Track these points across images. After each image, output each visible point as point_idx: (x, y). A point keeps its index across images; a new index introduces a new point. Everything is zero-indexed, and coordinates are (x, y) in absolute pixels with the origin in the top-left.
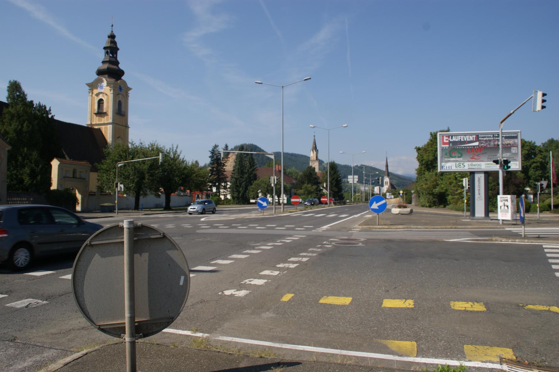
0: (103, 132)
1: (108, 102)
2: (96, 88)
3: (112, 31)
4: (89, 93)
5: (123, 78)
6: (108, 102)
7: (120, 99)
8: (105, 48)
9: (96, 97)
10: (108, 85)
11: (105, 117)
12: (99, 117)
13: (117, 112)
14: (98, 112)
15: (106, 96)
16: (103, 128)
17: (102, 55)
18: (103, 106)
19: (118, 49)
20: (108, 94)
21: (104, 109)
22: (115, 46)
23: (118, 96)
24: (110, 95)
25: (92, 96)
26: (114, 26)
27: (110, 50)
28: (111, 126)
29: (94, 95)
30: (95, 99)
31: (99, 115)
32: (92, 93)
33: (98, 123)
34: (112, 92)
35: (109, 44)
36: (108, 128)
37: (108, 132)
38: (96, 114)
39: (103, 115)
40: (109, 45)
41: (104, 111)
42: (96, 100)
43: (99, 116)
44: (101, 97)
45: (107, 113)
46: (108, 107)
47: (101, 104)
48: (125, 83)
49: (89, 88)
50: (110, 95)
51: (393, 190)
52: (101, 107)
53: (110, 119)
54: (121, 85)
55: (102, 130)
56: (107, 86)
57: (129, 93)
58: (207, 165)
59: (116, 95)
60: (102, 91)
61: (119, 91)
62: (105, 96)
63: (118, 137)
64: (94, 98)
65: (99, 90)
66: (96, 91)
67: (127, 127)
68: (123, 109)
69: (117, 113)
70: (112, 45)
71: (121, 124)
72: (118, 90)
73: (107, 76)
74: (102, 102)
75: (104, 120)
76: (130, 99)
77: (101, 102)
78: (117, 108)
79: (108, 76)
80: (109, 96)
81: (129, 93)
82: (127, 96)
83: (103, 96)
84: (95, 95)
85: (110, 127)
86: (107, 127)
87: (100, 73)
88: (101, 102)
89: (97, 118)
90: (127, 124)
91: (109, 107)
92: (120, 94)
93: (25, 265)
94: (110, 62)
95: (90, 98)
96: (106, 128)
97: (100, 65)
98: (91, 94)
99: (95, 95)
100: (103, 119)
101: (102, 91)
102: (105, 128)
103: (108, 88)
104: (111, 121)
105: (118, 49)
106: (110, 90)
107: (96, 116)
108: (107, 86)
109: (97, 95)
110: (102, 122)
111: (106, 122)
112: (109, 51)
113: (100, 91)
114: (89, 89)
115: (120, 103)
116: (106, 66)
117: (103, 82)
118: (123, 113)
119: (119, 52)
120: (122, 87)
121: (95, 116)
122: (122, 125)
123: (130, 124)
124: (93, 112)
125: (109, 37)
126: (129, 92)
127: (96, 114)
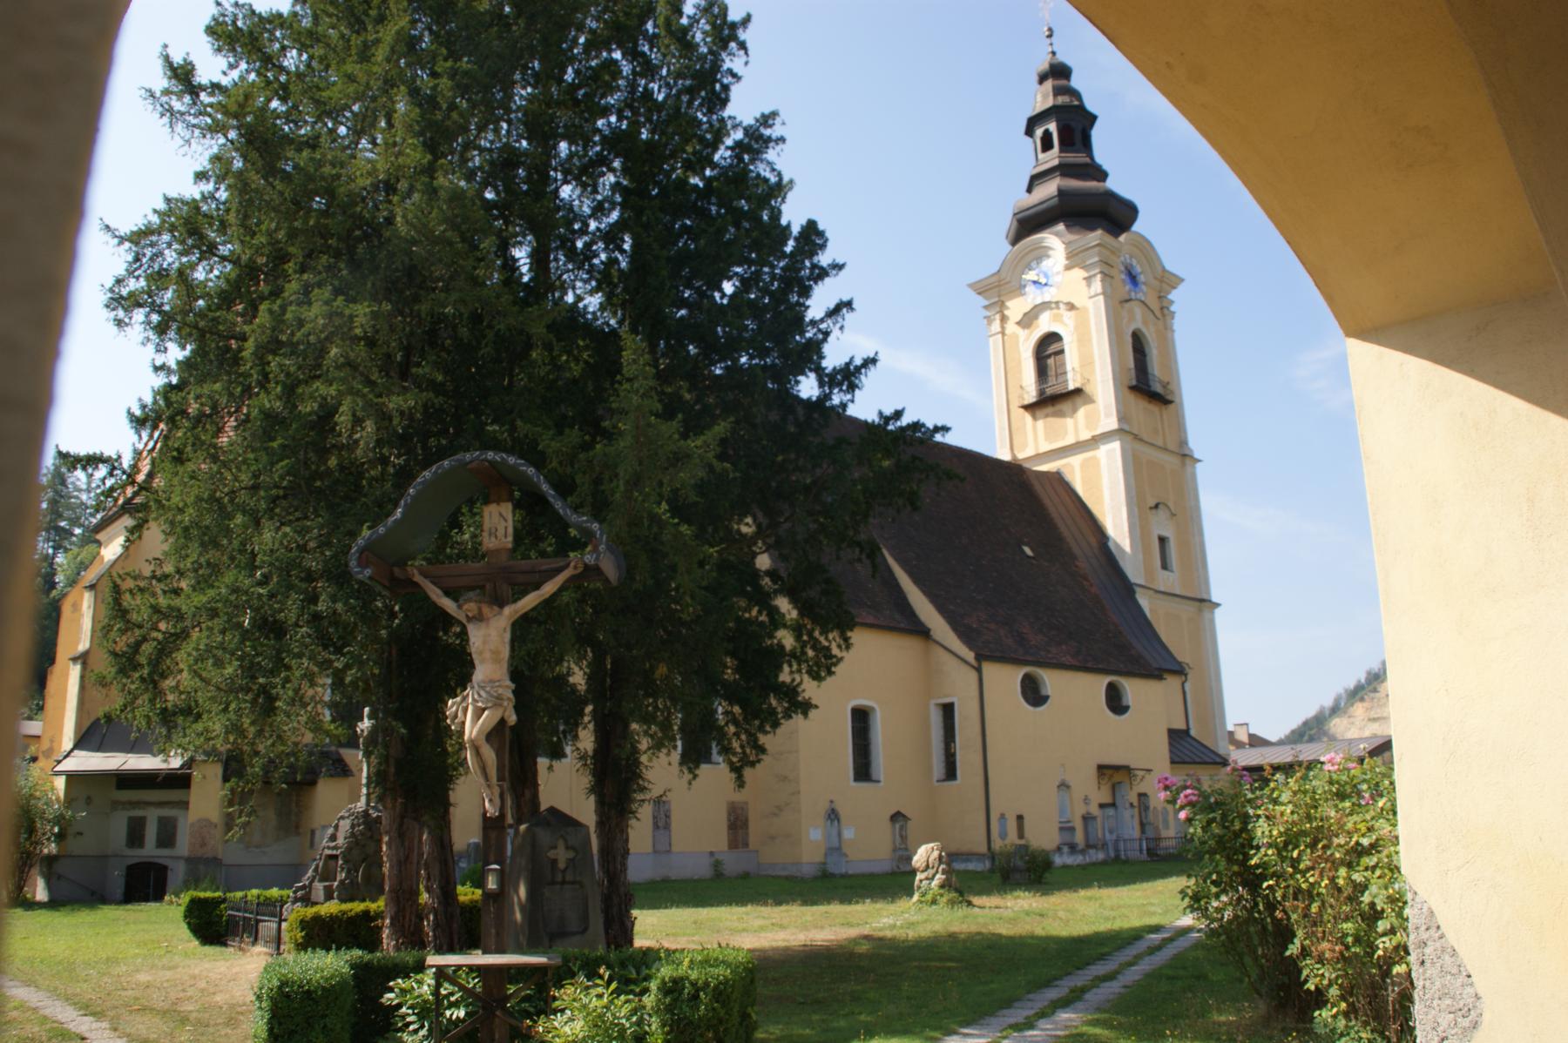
0: (1079, 488)
1: (1083, 339)
2: (1019, 289)
3: (1054, 53)
4: (989, 320)
5: (1136, 227)
6: (1083, 339)
7: (1138, 324)
8: (1032, 124)
9: (1022, 333)
10: (1075, 258)
11: (1082, 412)
12: (1051, 420)
13: (1134, 383)
14: (1041, 392)
15: (1073, 313)
16: (1075, 471)
17: (1026, 156)
18: (1063, 364)
19: (1092, 119)
20: (1077, 304)
21: (1070, 376)
22: (1076, 103)
23: (1127, 305)
24: (1090, 304)
25: (1003, 333)
26: (1055, 34)
27: (1058, 122)
28: (1115, 446)
29: (1011, 327)
30: (1017, 342)
31: (1050, 409)
32: (1004, 319)
33: (1045, 447)
34: (1097, 285)
35: (1051, 98)
36: (1103, 461)
37: (1105, 481)
38: (1028, 408)
39: (1065, 406)
40: (1050, 103)
41: (1071, 387)
42: (1027, 344)
43: (1047, 416)
44: (1045, 325)
45: (1088, 389)
46: (1086, 362)
47: (1051, 361)
48: (1145, 248)
49: (986, 303)
50: (1090, 304)
51: (268, 927)
52: (1051, 372)
53: (1107, 416)
54: (1134, 262)
55: (1068, 477)
56: (1068, 268)
57: (1172, 302)
58: (1327, 713)
59: (1116, 306)
60: (1047, 299)
61: (1128, 287)
62: (1068, 316)
63: (1156, 506)
64: (1016, 336)
65: (1032, 297)
66: (1016, 308)
67: (1185, 457)
68: (1156, 368)
69: (1133, 388)
70: (1061, 100)
71: (1160, 443)
72: (1123, 281)
73: (1061, 227)
74: (1053, 348)
75: (1075, 425)
76: (1179, 324)
77: (1047, 350)
78: (1131, 364)
79: (1067, 226)
80: (1085, 310)
81: (1172, 302)
82: (1163, 313)
83: (1058, 319)
84: (1018, 323)
85: (1111, 456)
86: (1095, 460)
87: (1029, 224)
88: (1047, 350)
89: (1040, 423)
90: (1183, 443)
91: (1092, 363)
92: (1130, 300)
93: (243, 66)
94: (1063, 170)
95: (995, 343)
96: (1091, 467)
97: (1017, 197)
98: (996, 326)
99: (1018, 323)
100: (1069, 421)
101: (1048, 295)
102: (1084, 465)
103: (1078, 274)
104: (1111, 423)
105: (1092, 119)
106: (1088, 279)
107: (1035, 418)
108: (1068, 268)
109: (1027, 320)
110: (1070, 440)
111: (1085, 435)
112: (1052, 127)
113: (1039, 301)
114: (986, 307)
115: (1139, 346)
116: (1049, 189)
117: (1048, 256)
118: (1158, 388)
119: (1097, 134)
120: (1139, 269)
121: (1028, 417)
122: (1166, 450)
123: (1196, 444)
124: (1015, 404)
125: (1042, 78)
126: (1170, 297)
127: (1028, 408)
